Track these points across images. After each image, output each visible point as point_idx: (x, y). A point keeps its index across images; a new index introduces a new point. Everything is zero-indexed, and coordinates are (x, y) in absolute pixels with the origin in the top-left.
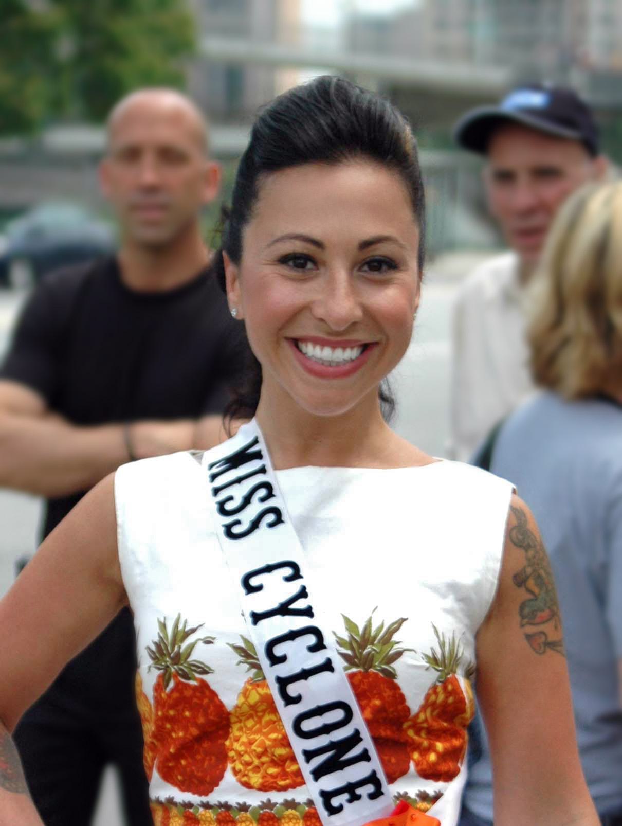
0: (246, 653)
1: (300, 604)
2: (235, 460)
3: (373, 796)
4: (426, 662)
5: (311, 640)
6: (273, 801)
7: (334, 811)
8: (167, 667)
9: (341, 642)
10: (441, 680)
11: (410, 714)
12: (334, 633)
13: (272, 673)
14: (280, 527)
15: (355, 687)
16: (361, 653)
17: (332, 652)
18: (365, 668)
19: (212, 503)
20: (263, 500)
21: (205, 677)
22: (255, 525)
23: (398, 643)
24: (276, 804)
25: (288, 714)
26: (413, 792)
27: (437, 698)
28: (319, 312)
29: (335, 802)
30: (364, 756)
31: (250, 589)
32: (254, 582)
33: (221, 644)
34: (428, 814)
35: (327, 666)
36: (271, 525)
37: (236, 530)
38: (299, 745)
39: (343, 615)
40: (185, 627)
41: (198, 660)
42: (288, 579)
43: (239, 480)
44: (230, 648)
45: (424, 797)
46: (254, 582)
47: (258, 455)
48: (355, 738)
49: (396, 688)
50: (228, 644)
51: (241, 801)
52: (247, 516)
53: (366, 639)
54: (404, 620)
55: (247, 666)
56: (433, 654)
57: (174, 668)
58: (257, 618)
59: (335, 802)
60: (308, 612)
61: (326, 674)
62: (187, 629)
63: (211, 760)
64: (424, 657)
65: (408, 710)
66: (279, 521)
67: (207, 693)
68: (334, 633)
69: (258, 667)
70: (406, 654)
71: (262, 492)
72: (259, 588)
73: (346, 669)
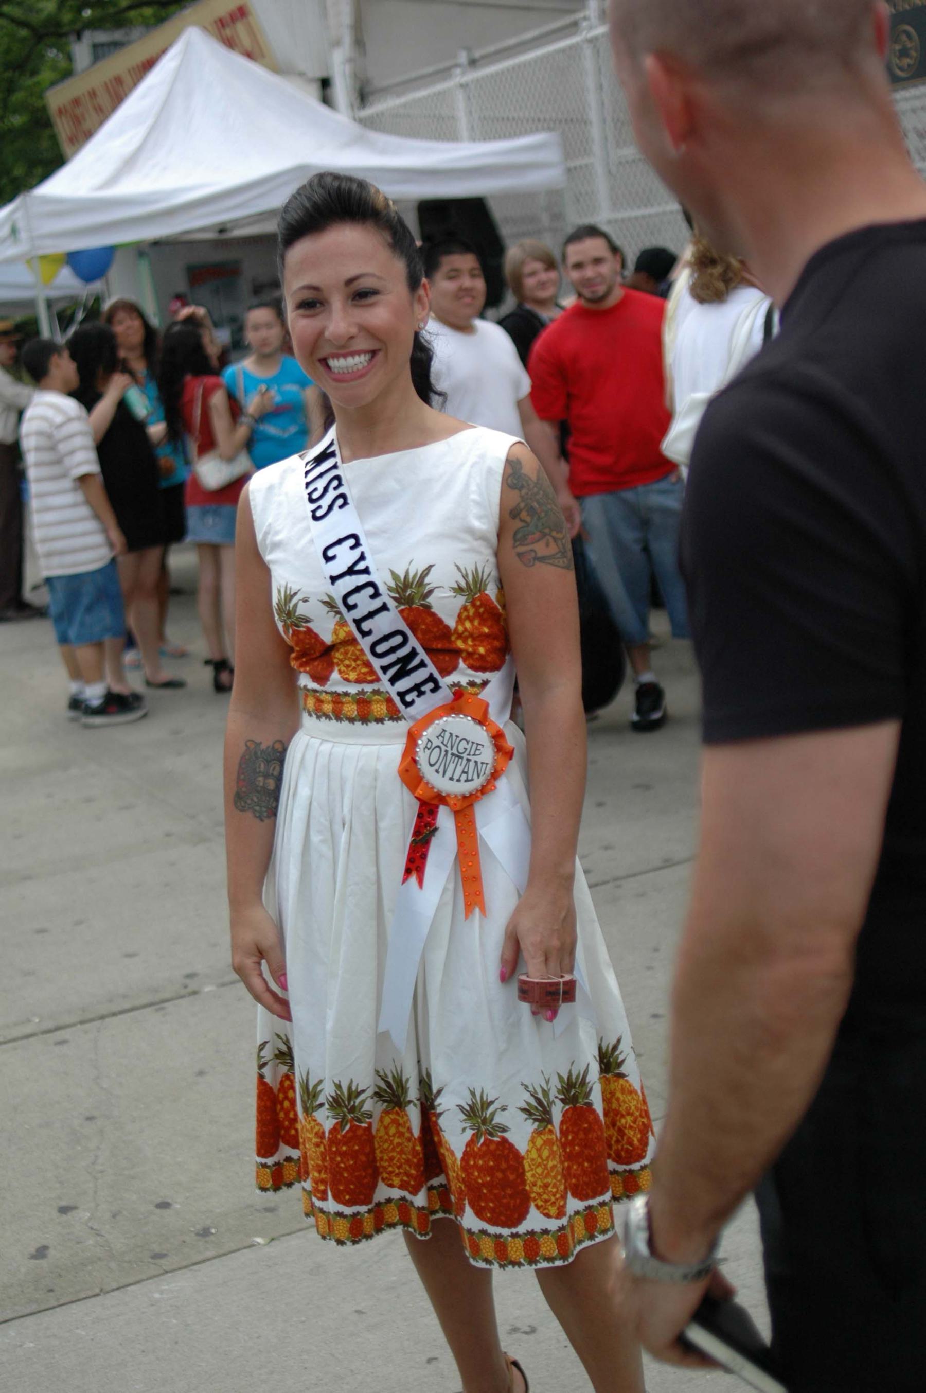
0: (330, 604)
2: (319, 460)
3: (433, 691)
4: (454, 593)
5: (370, 590)
6: (365, 690)
7: (408, 704)
9: (390, 589)
10: (468, 601)
11: (451, 630)
12: (385, 583)
13: (350, 617)
14: (347, 507)
15: (405, 619)
16: (405, 596)
17: (386, 597)
18: (409, 606)
19: (305, 494)
20: (335, 489)
21: (308, 625)
22: (330, 508)
23: (429, 584)
24: (367, 692)
25: (365, 643)
26: (464, 681)
27: (469, 613)
29: (408, 698)
30: (422, 664)
31: (328, 559)
32: (330, 553)
33: (313, 601)
34: (480, 696)
35: (384, 608)
36: (341, 507)
37: (319, 513)
38: (377, 663)
39: (390, 569)
40: (290, 592)
42: (352, 548)
43: (321, 475)
44: (320, 604)
45: (472, 684)
46: (330, 553)
47: (333, 454)
48: (413, 653)
49: (433, 615)
50: (319, 600)
51: (344, 690)
52: (325, 502)
53: (406, 585)
54: (431, 566)
56: (458, 585)
58: (334, 579)
59: (408, 698)
60: (366, 571)
61: (384, 613)
63: (323, 665)
64: (451, 589)
65: (447, 627)
66: (345, 503)
68: (385, 583)
69: (338, 613)
70: (436, 590)
71: (335, 483)
72: (334, 558)
73: (397, 607)
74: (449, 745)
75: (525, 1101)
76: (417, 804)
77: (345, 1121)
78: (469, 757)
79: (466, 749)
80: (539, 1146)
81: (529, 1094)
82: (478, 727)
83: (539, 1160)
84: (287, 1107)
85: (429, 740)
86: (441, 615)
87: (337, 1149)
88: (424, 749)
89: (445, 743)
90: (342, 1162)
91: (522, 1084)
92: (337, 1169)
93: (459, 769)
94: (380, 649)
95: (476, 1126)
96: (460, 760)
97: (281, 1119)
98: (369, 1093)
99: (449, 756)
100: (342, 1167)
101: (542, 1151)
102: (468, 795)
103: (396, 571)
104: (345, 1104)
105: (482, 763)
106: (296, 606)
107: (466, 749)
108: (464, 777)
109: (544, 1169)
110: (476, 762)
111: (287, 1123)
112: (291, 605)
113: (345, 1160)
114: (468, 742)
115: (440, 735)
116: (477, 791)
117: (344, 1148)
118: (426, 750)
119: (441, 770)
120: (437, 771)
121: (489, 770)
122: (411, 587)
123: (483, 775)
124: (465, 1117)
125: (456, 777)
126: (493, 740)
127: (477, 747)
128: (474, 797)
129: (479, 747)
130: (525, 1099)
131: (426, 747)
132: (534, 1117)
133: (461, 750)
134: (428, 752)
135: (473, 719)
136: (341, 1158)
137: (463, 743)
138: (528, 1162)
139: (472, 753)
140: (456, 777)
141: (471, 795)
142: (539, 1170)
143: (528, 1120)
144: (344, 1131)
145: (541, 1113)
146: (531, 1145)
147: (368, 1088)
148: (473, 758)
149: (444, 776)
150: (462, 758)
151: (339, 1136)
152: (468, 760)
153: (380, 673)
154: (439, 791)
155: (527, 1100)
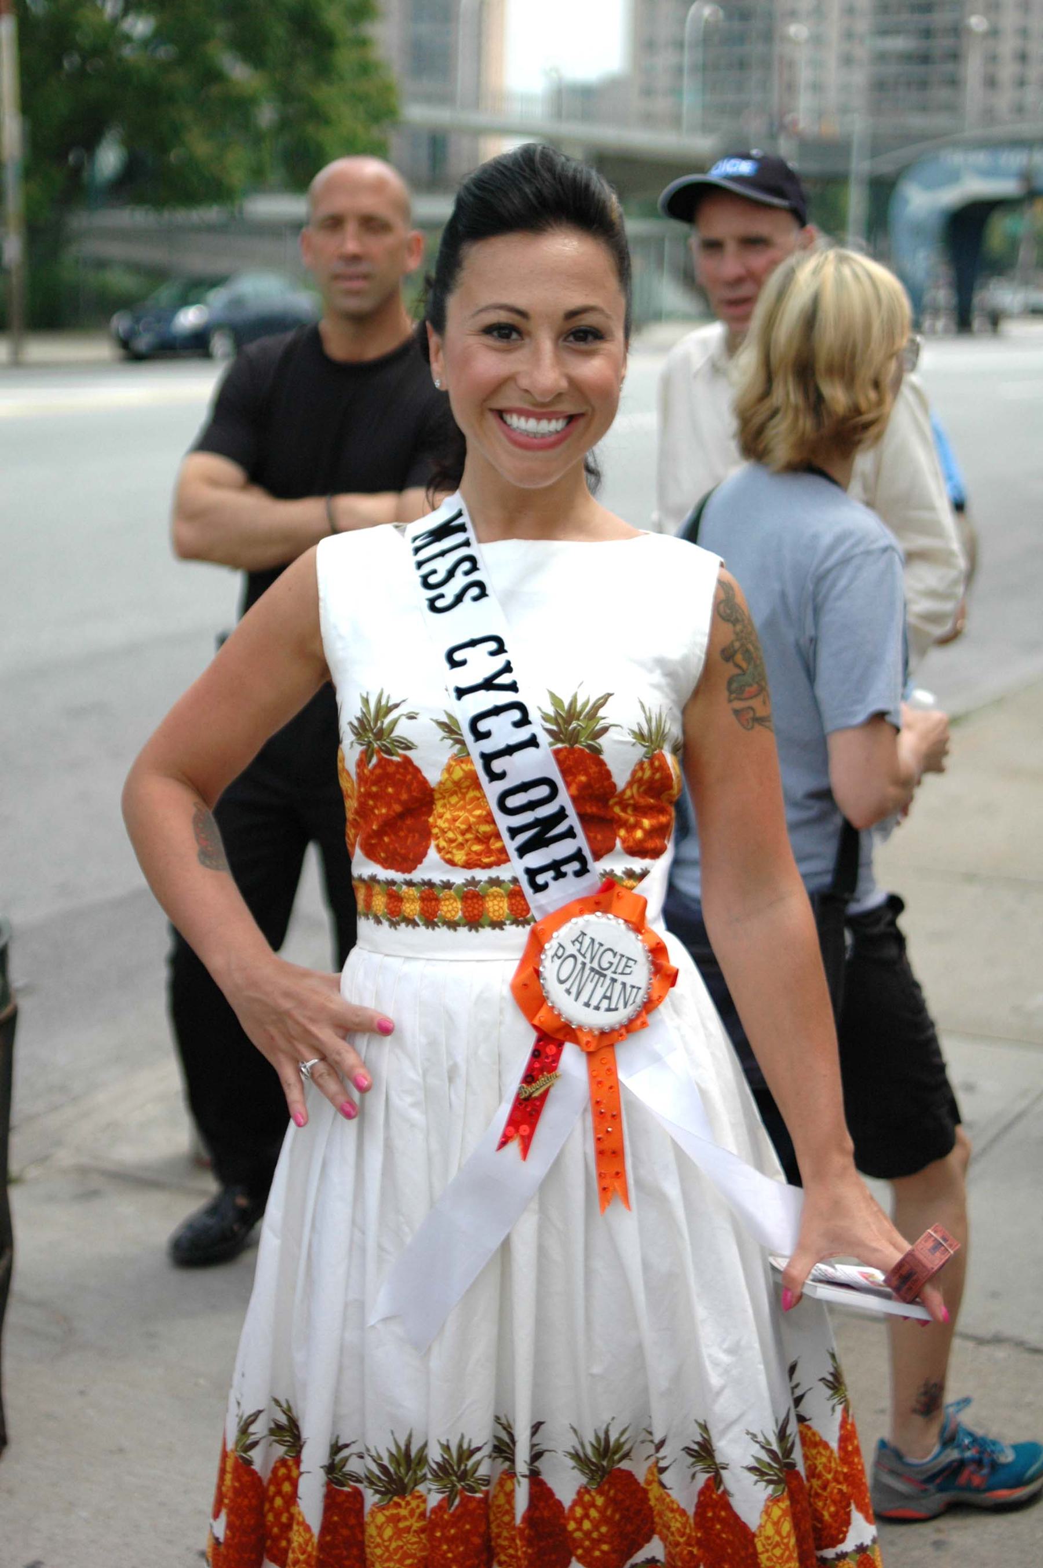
1: (505, 679)
3: (578, 874)
4: (633, 738)
5: (516, 715)
7: (538, 888)
8: (370, 742)
9: (546, 718)
12: (540, 709)
13: (476, 748)
15: (560, 763)
16: (567, 729)
17: (537, 727)
18: (570, 744)
21: (408, 753)
25: (492, 790)
28: (524, 382)
29: (540, 879)
30: (570, 833)
31: (454, 664)
32: (458, 656)
34: (635, 891)
36: (476, 599)
38: (504, 822)
39: (548, 691)
40: (388, 702)
41: (402, 735)
42: (493, 654)
43: (443, 554)
44: (434, 724)
45: (630, 874)
46: (458, 656)
47: (462, 528)
48: (561, 815)
49: (602, 764)
50: (432, 720)
53: (572, 714)
54: (610, 695)
55: (451, 742)
56: (640, 730)
57: (377, 744)
58: (461, 693)
59: (540, 879)
60: (513, 687)
61: (531, 750)
62: (390, 704)
64: (630, 732)
65: (614, 786)
66: (483, 594)
67: (410, 769)
68: (540, 709)
69: (462, 743)
70: (612, 729)
72: (463, 663)
73: (551, 744)
74: (588, 955)
75: (753, 1456)
76: (532, 1037)
77: (454, 1493)
78: (615, 976)
79: (611, 964)
80: (775, 1519)
81: (758, 1446)
82: (632, 935)
83: (777, 1538)
84: (279, 1506)
85: (561, 946)
86: (611, 766)
87: (443, 1534)
88: (553, 957)
89: (583, 951)
90: (449, 1550)
91: (748, 1433)
92: (442, 1562)
93: (600, 992)
94: (512, 802)
95: (712, 1468)
96: (602, 979)
97: (269, 1524)
98: (487, 1450)
99: (587, 971)
100: (448, 1558)
101: (781, 1524)
102: (607, 1029)
103: (559, 694)
104: (453, 1469)
105: (633, 987)
106: (395, 722)
107: (611, 964)
108: (605, 1004)
109: (785, 1550)
110: (624, 984)
111: (276, 1530)
112: (387, 721)
113: (453, 1547)
114: (615, 954)
115: (577, 940)
116: (622, 1026)
117: (453, 1531)
118: (555, 958)
119: (574, 990)
120: (568, 992)
121: (641, 997)
122: (578, 719)
123: (632, 1004)
124: (692, 1460)
125: (594, 1002)
126: (649, 954)
127: (626, 963)
128: (616, 1034)
129: (631, 963)
130: (753, 1453)
131: (556, 954)
132: (766, 1478)
133: (605, 965)
134: (558, 962)
135: (626, 921)
136: (448, 1545)
137: (609, 956)
138: (760, 1540)
139: (620, 970)
140: (594, 1002)
141: (613, 1030)
142: (778, 1552)
143: (759, 1483)
144: (453, 1508)
145: (777, 1471)
146: (765, 1517)
147: (485, 1444)
148: (621, 978)
149: (576, 999)
150: (605, 976)
151: (446, 1517)
152: (614, 980)
153: (505, 835)
154: (567, 1020)
155: (756, 1455)
